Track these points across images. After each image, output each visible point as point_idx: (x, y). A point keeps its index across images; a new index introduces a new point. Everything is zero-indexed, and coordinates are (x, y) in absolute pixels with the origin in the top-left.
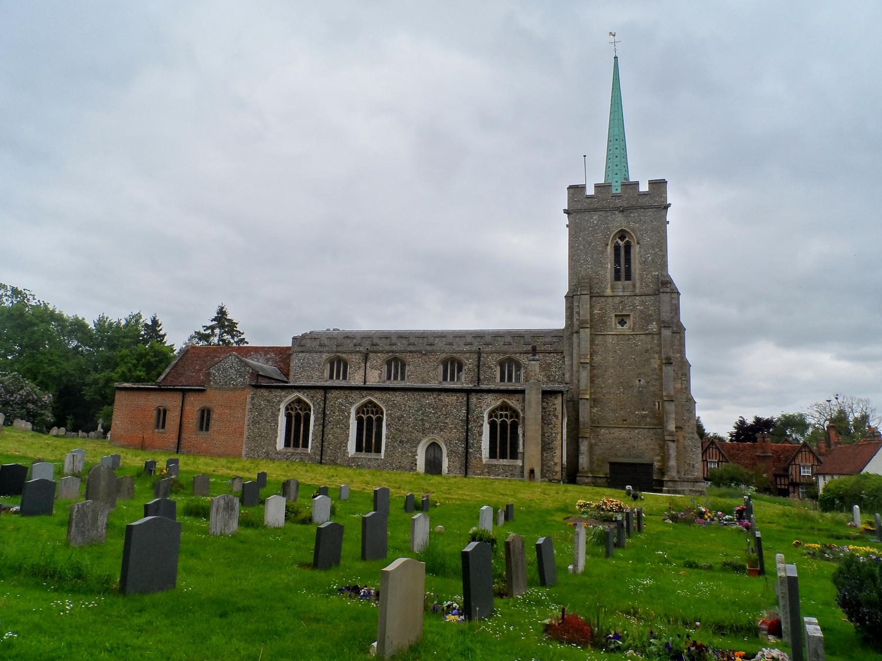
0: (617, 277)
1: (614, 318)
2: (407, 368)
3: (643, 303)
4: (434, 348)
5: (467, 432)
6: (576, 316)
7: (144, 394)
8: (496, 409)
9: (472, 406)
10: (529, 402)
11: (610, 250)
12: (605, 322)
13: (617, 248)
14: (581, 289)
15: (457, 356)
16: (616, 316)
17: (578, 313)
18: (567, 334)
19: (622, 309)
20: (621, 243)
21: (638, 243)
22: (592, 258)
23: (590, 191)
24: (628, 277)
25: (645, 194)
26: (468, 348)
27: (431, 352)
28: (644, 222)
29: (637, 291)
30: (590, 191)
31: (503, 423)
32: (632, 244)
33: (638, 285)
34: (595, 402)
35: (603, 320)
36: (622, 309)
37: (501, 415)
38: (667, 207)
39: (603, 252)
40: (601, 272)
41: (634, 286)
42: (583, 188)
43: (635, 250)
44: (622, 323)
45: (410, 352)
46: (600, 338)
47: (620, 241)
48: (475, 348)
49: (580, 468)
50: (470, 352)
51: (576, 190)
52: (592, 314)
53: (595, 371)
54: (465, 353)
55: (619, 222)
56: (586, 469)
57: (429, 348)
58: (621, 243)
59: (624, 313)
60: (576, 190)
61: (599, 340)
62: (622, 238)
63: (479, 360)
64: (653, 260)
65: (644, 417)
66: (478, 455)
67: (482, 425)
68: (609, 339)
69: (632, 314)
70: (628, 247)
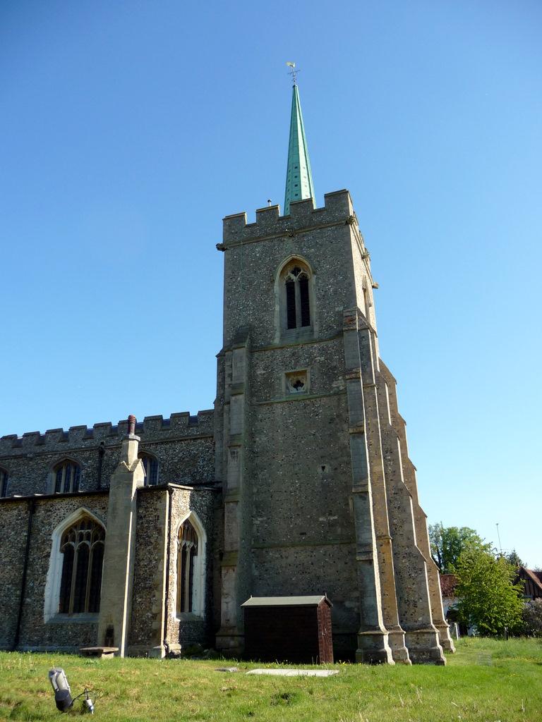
0: (291, 324)
1: (283, 379)
2: (9, 481)
3: (323, 351)
4: (44, 448)
5: (25, 569)
6: (228, 381)
7: (194, 595)
8: (75, 526)
9: (37, 524)
10: (114, 509)
11: (279, 289)
12: (271, 386)
13: (290, 286)
14: (241, 339)
15: (71, 457)
16: (288, 375)
17: (230, 375)
18: (237, 420)
19: (296, 365)
20: (295, 278)
21: (314, 273)
22: (254, 301)
23: (250, 219)
24: (306, 321)
25: (320, 211)
26: (88, 443)
27: (39, 455)
28: (321, 245)
29: (316, 336)
30: (250, 219)
31: (83, 549)
32: (309, 277)
33: (316, 328)
34: (257, 507)
35: (268, 384)
36: (296, 365)
37: (81, 535)
38: (349, 221)
39: (268, 291)
40: (267, 318)
41: (312, 331)
42: (242, 216)
43: (313, 281)
44: (298, 384)
45: (15, 457)
46: (264, 409)
47: (293, 276)
48: (96, 443)
49: (223, 622)
50: (90, 449)
51: (232, 222)
52: (251, 377)
53: (258, 461)
54: (84, 451)
55: (288, 250)
56: (232, 622)
57: (38, 449)
58: (295, 278)
59: (299, 369)
60: (232, 222)
61: (263, 412)
62: (296, 271)
63: (101, 462)
64: (335, 292)
65: (332, 525)
66: (38, 609)
67: (48, 555)
68: (278, 409)
69: (309, 369)
70: (304, 282)
